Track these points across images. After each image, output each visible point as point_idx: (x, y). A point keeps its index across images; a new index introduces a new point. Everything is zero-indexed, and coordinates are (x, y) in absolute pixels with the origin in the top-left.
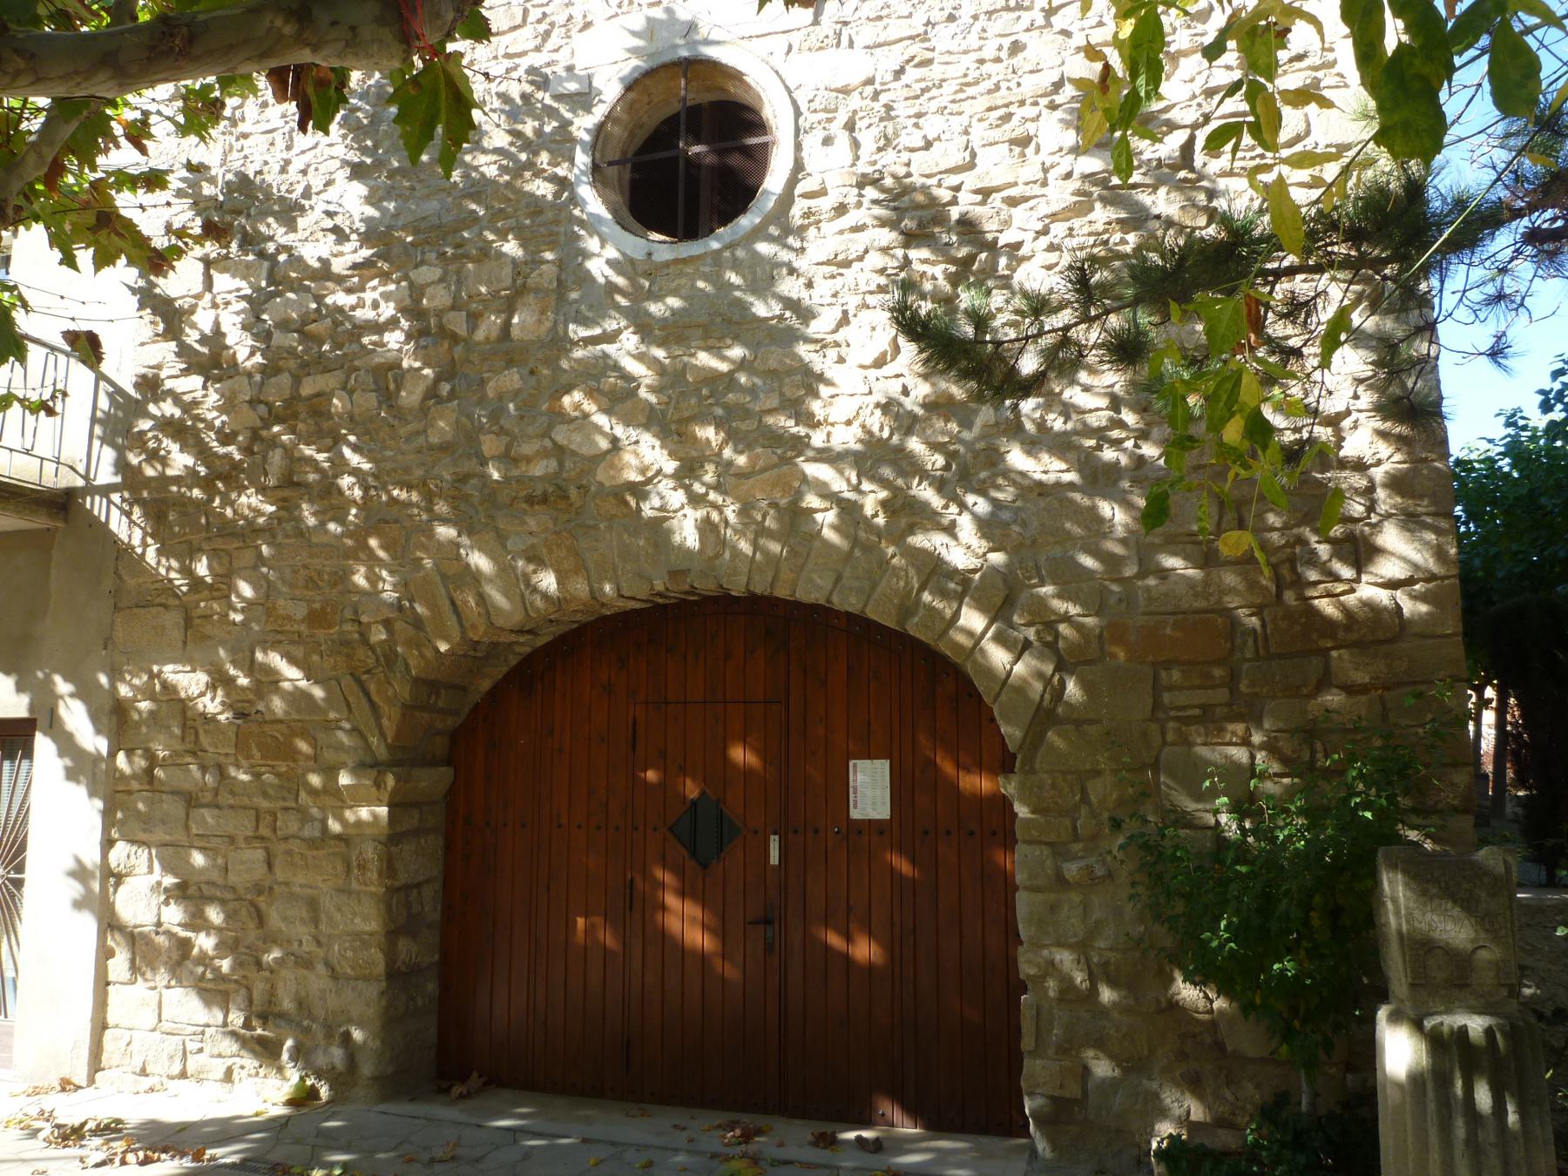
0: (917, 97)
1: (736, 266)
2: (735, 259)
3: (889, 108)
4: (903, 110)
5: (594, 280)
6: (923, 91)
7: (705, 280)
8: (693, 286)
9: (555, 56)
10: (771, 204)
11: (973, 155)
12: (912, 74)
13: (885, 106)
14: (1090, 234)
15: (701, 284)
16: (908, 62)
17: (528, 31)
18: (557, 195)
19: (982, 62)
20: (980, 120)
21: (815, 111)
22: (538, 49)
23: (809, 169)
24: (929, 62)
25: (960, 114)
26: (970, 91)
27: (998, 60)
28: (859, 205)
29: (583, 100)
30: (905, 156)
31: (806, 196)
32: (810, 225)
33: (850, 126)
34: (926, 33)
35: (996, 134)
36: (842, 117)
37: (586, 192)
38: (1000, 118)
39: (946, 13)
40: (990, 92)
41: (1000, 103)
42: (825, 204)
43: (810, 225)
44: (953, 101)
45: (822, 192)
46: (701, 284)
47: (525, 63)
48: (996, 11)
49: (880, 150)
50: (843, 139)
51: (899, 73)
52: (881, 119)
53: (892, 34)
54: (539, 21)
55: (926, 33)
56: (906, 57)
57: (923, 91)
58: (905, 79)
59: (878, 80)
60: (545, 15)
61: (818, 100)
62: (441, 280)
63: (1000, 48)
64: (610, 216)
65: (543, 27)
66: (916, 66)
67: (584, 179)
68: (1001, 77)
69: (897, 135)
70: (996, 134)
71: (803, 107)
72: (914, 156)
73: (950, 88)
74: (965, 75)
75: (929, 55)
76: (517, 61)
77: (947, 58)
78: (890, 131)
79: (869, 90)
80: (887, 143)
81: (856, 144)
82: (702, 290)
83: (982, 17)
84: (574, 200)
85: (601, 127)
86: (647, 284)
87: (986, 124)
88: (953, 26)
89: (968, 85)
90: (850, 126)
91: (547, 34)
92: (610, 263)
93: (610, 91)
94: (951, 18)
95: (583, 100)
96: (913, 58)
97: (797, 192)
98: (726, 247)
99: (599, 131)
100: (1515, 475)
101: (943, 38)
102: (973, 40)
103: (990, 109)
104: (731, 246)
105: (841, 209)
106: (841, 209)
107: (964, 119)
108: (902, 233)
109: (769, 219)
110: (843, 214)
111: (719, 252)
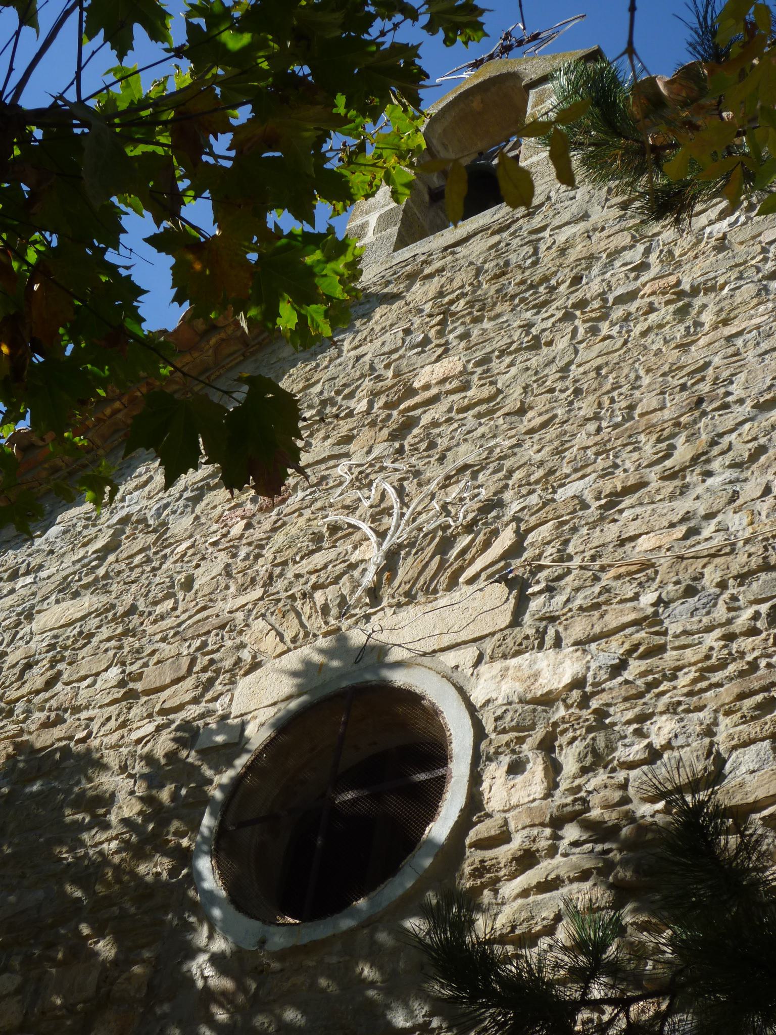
0: (641, 695)
1: (374, 955)
2: (373, 942)
3: (601, 714)
4: (621, 715)
5: (192, 982)
6: (650, 686)
7: (329, 977)
8: (313, 984)
9: (211, 706)
10: (427, 862)
11: (720, 762)
12: (635, 666)
13: (596, 711)
14: (731, 268)
15: (323, 982)
16: (630, 652)
17: (190, 682)
18: (173, 872)
19: (730, 637)
20: (727, 713)
21: (504, 731)
22: (196, 701)
23: (489, 808)
24: (660, 649)
25: (700, 709)
26: (716, 677)
27: (753, 632)
28: (552, 851)
29: (222, 756)
30: (621, 776)
31: (481, 844)
32: (484, 886)
33: (547, 746)
34: (656, 614)
35: (752, 730)
36: (539, 733)
37: (205, 864)
38: (758, 707)
39: (682, 587)
40: (742, 674)
41: (756, 685)
42: (504, 853)
43: (484, 886)
44: (690, 694)
45: (504, 837)
46: (323, 982)
47: (179, 718)
48: (751, 573)
49: (584, 771)
50: (536, 768)
51: (617, 669)
52: (590, 730)
53: (612, 620)
54: (204, 670)
55: (656, 614)
56: (627, 646)
57: (650, 686)
58: (627, 675)
59: (590, 680)
60: (212, 662)
61: (508, 718)
62: (19, 991)
63: (756, 616)
64: (223, 894)
65: (204, 677)
66: (642, 657)
67: (205, 848)
68: (757, 653)
69: (611, 748)
70: (752, 730)
71: (489, 726)
72: (633, 774)
73: (684, 680)
74: (708, 657)
75: (659, 640)
76: (171, 717)
77: (684, 640)
78: (601, 743)
79: (576, 694)
80: (595, 760)
81: (554, 768)
82: (323, 991)
83: (731, 582)
84: (194, 878)
85: (238, 781)
86: (254, 986)
87: (736, 717)
88: (692, 602)
89: (713, 669)
90: (547, 746)
91: (211, 682)
92: (217, 960)
93: (257, 735)
94: (691, 591)
95: (238, 744)
96: (635, 647)
97: (468, 841)
98: (362, 926)
99: (234, 788)
100: (242, 115)
101: (677, 621)
102: (721, 612)
103: (742, 696)
104: (371, 923)
105: (526, 860)
106: (526, 860)
107: (705, 716)
108: (610, 887)
109: (425, 881)
110: (531, 866)
111: (352, 931)
